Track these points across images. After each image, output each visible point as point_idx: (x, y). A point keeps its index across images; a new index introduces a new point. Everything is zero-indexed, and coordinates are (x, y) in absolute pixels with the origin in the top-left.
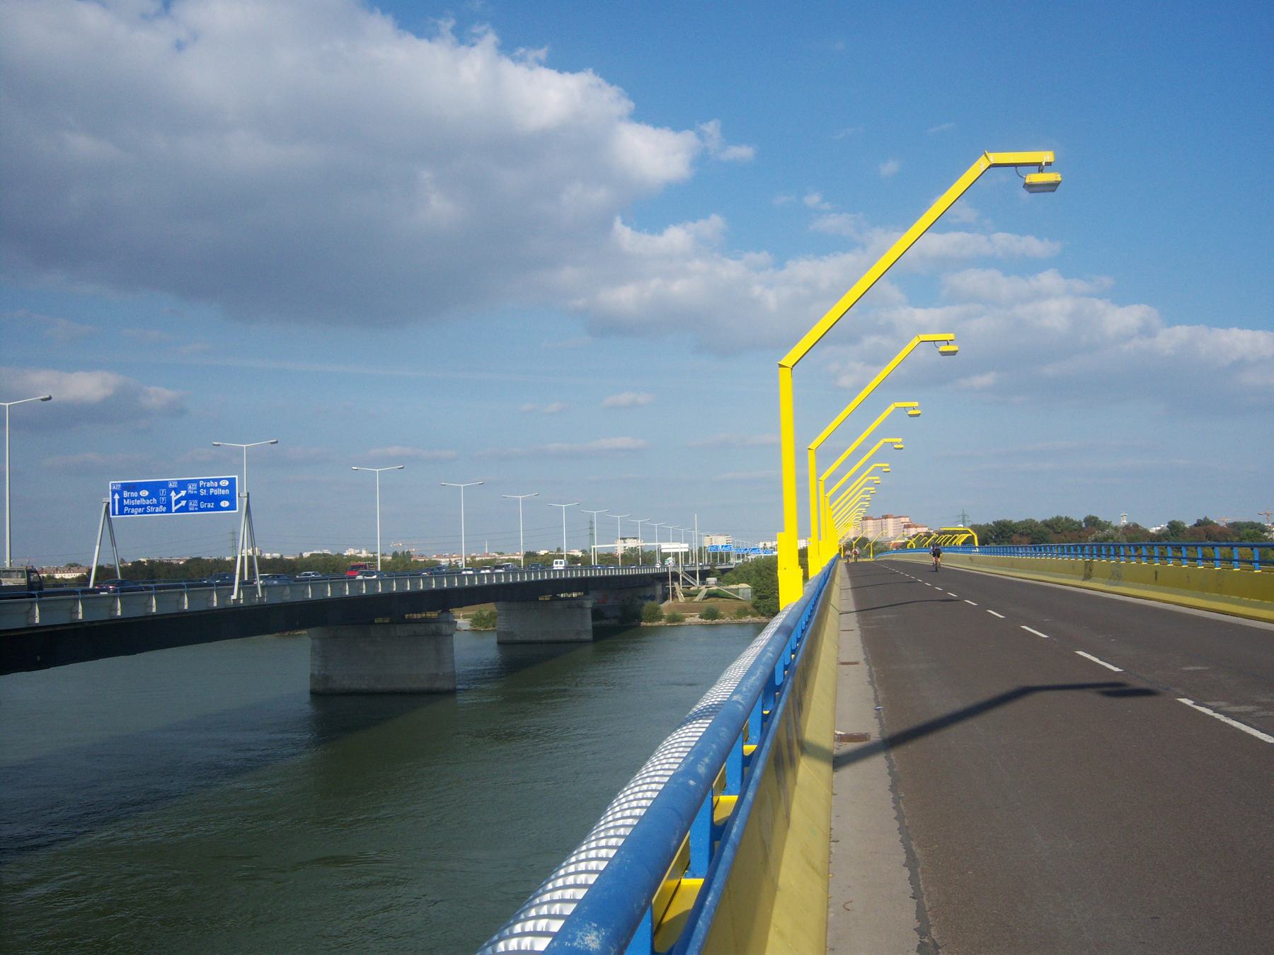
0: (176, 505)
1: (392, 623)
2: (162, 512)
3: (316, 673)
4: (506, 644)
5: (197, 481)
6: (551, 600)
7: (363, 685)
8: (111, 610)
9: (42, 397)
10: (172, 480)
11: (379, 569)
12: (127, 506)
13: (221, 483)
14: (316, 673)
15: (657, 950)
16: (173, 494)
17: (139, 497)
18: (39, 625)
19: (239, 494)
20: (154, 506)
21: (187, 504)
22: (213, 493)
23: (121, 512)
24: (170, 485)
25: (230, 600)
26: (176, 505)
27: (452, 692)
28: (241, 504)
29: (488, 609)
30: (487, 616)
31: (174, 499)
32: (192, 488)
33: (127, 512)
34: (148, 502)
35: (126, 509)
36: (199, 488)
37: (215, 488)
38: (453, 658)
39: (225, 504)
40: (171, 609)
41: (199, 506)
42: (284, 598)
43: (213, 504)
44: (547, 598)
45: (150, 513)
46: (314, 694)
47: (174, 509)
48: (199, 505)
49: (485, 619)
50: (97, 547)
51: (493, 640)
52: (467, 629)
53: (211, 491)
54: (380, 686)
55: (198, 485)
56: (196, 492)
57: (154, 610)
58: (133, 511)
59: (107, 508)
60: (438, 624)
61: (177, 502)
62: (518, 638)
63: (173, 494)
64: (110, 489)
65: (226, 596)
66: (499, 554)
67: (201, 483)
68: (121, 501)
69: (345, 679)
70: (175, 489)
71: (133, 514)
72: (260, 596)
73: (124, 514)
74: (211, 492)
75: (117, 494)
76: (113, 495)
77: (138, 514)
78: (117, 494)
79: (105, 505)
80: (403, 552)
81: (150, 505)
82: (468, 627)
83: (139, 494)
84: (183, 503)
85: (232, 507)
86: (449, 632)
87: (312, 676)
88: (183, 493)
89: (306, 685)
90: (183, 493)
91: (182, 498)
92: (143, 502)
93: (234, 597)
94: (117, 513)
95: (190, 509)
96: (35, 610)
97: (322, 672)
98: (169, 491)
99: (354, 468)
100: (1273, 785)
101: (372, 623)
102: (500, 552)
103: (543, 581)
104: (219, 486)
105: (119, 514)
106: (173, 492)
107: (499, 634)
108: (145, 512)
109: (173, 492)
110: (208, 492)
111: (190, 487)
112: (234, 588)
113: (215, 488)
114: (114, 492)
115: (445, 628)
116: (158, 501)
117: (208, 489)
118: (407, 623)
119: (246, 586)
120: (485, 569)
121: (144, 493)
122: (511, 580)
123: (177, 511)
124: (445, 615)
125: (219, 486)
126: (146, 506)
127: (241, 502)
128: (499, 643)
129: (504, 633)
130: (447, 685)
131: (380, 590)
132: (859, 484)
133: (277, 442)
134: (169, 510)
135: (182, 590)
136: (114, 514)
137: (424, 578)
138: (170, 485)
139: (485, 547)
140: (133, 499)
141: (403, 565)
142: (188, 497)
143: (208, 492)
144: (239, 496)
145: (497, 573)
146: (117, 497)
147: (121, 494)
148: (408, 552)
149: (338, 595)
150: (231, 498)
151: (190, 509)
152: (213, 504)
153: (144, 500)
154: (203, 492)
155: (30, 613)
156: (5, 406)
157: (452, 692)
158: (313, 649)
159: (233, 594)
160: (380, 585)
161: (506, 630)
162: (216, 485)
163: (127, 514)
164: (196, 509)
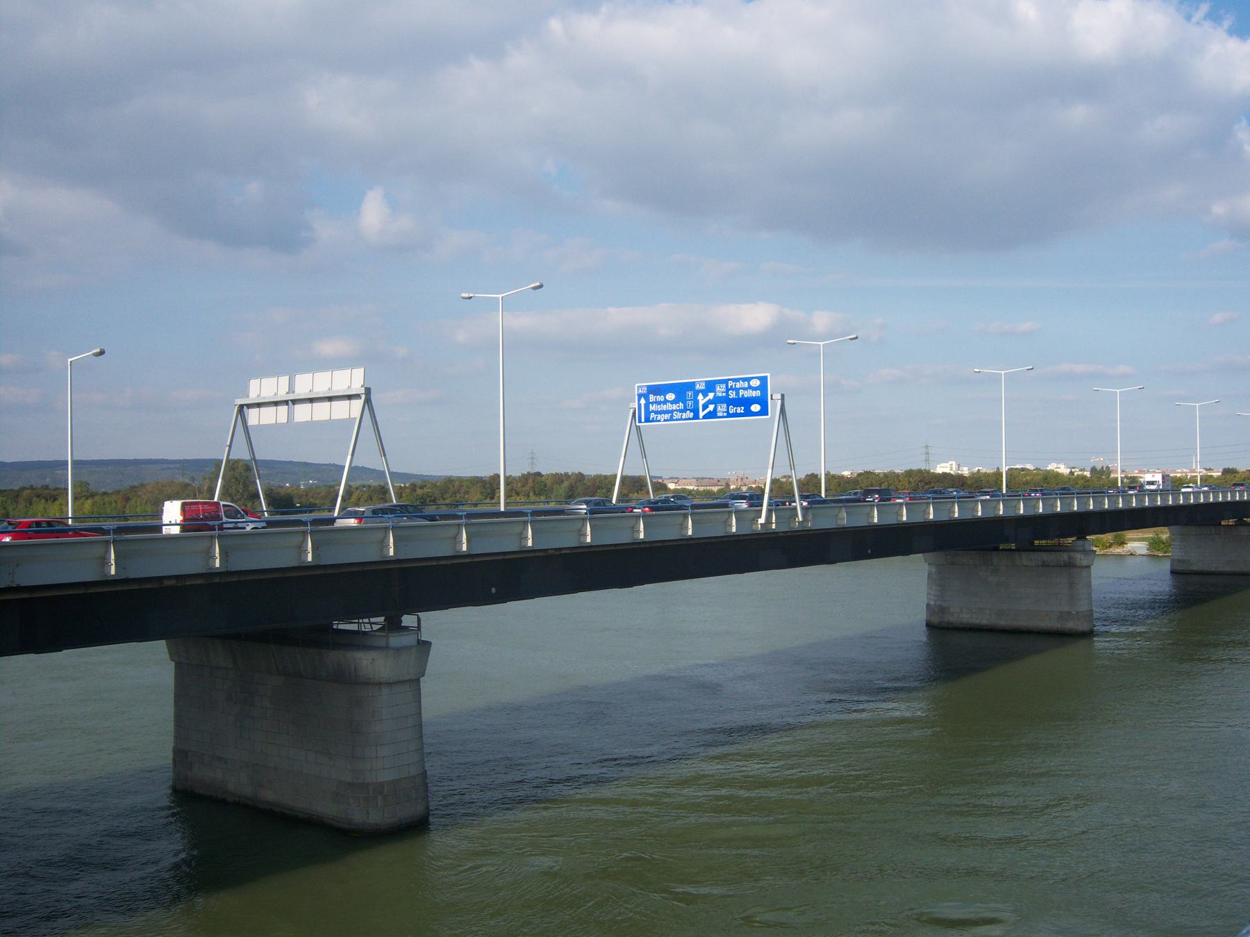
0: (703, 411)
1: (1017, 550)
2: (690, 419)
3: (932, 603)
4: (1183, 574)
5: (726, 382)
6: (1236, 525)
7: (983, 620)
8: (522, 539)
9: (533, 285)
10: (700, 381)
11: (1004, 492)
12: (653, 411)
13: (751, 383)
14: (932, 603)
16: (700, 397)
17: (665, 402)
18: (762, 532)
19: (772, 396)
20: (681, 411)
21: (715, 409)
22: (743, 395)
23: (647, 420)
24: (698, 387)
25: (757, 524)
26: (703, 411)
27: (1088, 634)
28: (774, 407)
29: (1164, 534)
30: (1166, 539)
32: (720, 390)
33: (653, 418)
34: (675, 407)
35: (652, 415)
36: (728, 390)
37: (745, 389)
38: (1090, 594)
39: (756, 408)
40: (944, 517)
41: (728, 412)
42: (839, 522)
43: (743, 408)
44: (1231, 522)
45: (677, 420)
46: (175, 790)
47: (702, 414)
48: (728, 409)
49: (1164, 543)
50: (622, 459)
51: (1166, 566)
52: (1144, 554)
53: (741, 392)
54: (1003, 623)
55: (727, 386)
56: (724, 394)
57: (876, 520)
58: (659, 417)
59: (634, 413)
60: (1072, 554)
61: (705, 407)
62: (1195, 568)
63: (700, 397)
64: (636, 393)
65: (753, 520)
66: (1207, 470)
67: (730, 383)
68: (647, 406)
69: (962, 613)
70: (702, 391)
71: (659, 421)
72: (801, 519)
73: (651, 422)
74: (741, 394)
75: (642, 398)
76: (639, 400)
77: (665, 420)
78: (642, 398)
79: (632, 411)
80: (1103, 467)
81: (676, 410)
82: (1145, 552)
83: (665, 398)
84: (711, 407)
85: (764, 411)
86: (1085, 563)
87: (928, 605)
88: (711, 396)
89: (921, 616)
90: (711, 396)
91: (710, 402)
92: (669, 407)
93: (762, 520)
94: (643, 420)
95: (719, 414)
96: (772, 517)
97: (938, 603)
98: (696, 393)
99: (975, 370)
101: (996, 549)
102: (1208, 468)
103: (999, 521)
104: (750, 387)
105: (645, 422)
106: (700, 394)
107: (1173, 562)
108: (671, 419)
109: (700, 394)
110: (737, 394)
111: (718, 389)
112: (761, 510)
113: (745, 389)
114: (640, 396)
115: (1080, 558)
116: (685, 406)
117: (737, 390)
118: (1034, 551)
119: (935, 501)
120: (900, 498)
121: (671, 396)
122: (1192, 501)
123: (705, 417)
124: (1080, 543)
125: (750, 387)
126: (673, 411)
127: (774, 406)
128: (1173, 572)
129: (1179, 561)
130: (1082, 626)
131: (1134, 505)
133: (857, 338)
134: (696, 417)
135: (954, 500)
136: (640, 422)
137: (739, 512)
138: (698, 387)
139: (1192, 462)
141: (1082, 481)
142: (716, 401)
143: (737, 394)
144: (772, 399)
145: (1183, 493)
146: (643, 401)
147: (647, 398)
148: (1108, 468)
149: (1066, 511)
150: (763, 402)
151: (719, 414)
152: (743, 408)
153: (670, 405)
154: (732, 395)
155: (456, 539)
156: (1001, 374)
157: (1088, 634)
158: (930, 575)
159: (760, 518)
160: (980, 507)
161: (1181, 558)
162: (746, 385)
163: (653, 421)
164: (725, 414)
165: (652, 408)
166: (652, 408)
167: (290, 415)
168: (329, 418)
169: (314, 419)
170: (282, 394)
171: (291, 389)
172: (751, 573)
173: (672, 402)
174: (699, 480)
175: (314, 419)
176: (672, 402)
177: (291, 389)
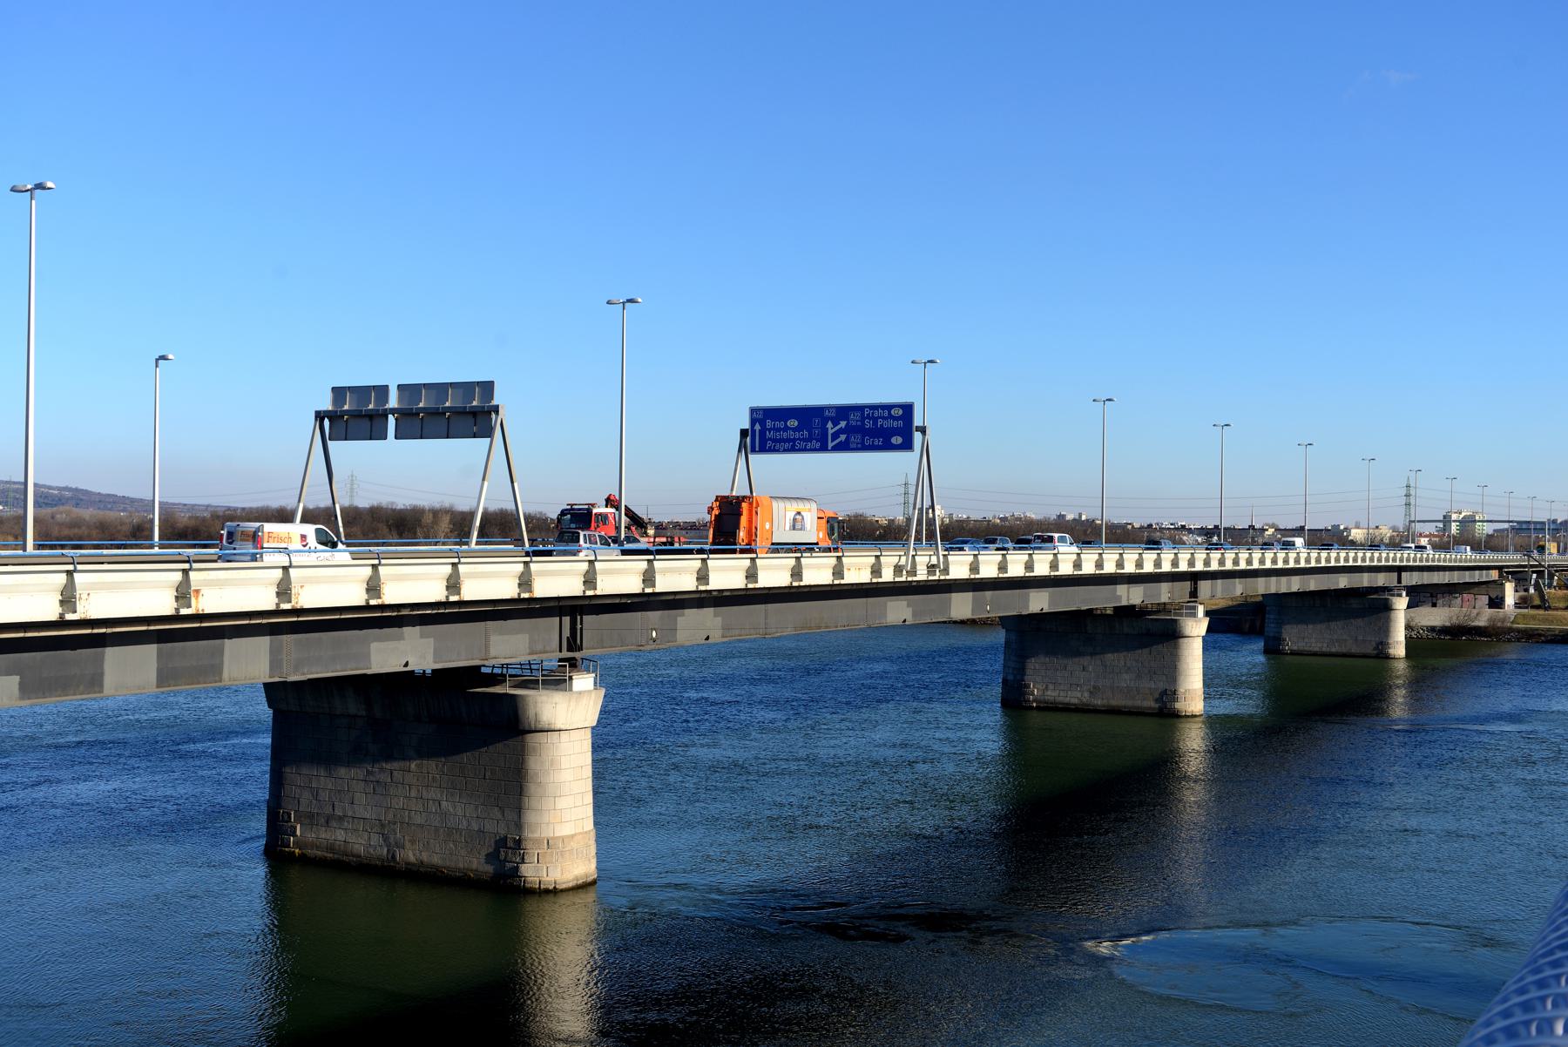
12: (770, 439)
16: (830, 425)
31: (830, 432)
35: (769, 444)
36: (863, 418)
39: (897, 440)
63: (830, 425)
84: (843, 437)
94: (757, 449)
125: (786, 428)
140: (778, 430)
147: (762, 423)
154: (868, 424)
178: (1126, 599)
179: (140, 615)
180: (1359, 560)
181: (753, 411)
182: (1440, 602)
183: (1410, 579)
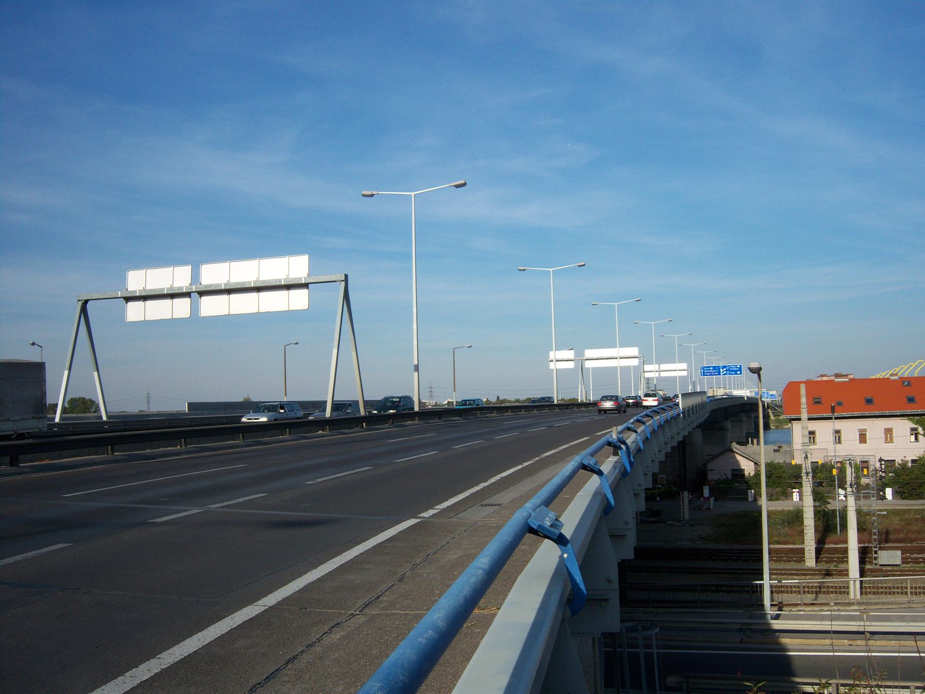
15: (89, 302)
16: (721, 369)
17: (710, 370)
31: (721, 371)
36: (730, 368)
39: (738, 372)
47: (722, 374)
63: (721, 369)
68: (703, 372)
72: (776, 582)
84: (725, 372)
85: (741, 374)
90: (725, 369)
92: (711, 371)
94: (772, 546)
100: (186, 693)
121: (711, 368)
125: (710, 370)
132: (720, 623)
146: (702, 370)
147: (703, 369)
154: (731, 369)
165: (706, 371)
166: (706, 371)
167: (195, 309)
168: (143, 319)
169: (146, 320)
170: (657, 369)
171: (659, 369)
172: (585, 508)
173: (712, 370)
174: (864, 590)
175: (146, 320)
176: (712, 370)
177: (659, 369)
178: (559, 357)
179: (524, 640)
180: (812, 438)
181: (44, 363)
182: (507, 542)
183: (903, 599)
